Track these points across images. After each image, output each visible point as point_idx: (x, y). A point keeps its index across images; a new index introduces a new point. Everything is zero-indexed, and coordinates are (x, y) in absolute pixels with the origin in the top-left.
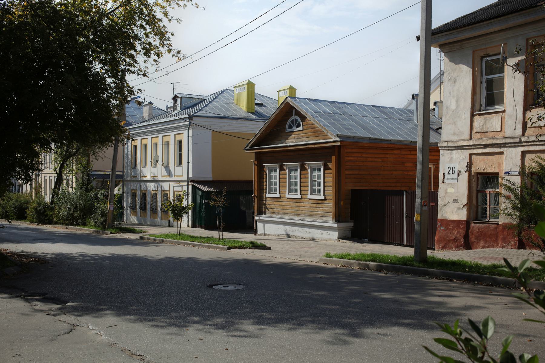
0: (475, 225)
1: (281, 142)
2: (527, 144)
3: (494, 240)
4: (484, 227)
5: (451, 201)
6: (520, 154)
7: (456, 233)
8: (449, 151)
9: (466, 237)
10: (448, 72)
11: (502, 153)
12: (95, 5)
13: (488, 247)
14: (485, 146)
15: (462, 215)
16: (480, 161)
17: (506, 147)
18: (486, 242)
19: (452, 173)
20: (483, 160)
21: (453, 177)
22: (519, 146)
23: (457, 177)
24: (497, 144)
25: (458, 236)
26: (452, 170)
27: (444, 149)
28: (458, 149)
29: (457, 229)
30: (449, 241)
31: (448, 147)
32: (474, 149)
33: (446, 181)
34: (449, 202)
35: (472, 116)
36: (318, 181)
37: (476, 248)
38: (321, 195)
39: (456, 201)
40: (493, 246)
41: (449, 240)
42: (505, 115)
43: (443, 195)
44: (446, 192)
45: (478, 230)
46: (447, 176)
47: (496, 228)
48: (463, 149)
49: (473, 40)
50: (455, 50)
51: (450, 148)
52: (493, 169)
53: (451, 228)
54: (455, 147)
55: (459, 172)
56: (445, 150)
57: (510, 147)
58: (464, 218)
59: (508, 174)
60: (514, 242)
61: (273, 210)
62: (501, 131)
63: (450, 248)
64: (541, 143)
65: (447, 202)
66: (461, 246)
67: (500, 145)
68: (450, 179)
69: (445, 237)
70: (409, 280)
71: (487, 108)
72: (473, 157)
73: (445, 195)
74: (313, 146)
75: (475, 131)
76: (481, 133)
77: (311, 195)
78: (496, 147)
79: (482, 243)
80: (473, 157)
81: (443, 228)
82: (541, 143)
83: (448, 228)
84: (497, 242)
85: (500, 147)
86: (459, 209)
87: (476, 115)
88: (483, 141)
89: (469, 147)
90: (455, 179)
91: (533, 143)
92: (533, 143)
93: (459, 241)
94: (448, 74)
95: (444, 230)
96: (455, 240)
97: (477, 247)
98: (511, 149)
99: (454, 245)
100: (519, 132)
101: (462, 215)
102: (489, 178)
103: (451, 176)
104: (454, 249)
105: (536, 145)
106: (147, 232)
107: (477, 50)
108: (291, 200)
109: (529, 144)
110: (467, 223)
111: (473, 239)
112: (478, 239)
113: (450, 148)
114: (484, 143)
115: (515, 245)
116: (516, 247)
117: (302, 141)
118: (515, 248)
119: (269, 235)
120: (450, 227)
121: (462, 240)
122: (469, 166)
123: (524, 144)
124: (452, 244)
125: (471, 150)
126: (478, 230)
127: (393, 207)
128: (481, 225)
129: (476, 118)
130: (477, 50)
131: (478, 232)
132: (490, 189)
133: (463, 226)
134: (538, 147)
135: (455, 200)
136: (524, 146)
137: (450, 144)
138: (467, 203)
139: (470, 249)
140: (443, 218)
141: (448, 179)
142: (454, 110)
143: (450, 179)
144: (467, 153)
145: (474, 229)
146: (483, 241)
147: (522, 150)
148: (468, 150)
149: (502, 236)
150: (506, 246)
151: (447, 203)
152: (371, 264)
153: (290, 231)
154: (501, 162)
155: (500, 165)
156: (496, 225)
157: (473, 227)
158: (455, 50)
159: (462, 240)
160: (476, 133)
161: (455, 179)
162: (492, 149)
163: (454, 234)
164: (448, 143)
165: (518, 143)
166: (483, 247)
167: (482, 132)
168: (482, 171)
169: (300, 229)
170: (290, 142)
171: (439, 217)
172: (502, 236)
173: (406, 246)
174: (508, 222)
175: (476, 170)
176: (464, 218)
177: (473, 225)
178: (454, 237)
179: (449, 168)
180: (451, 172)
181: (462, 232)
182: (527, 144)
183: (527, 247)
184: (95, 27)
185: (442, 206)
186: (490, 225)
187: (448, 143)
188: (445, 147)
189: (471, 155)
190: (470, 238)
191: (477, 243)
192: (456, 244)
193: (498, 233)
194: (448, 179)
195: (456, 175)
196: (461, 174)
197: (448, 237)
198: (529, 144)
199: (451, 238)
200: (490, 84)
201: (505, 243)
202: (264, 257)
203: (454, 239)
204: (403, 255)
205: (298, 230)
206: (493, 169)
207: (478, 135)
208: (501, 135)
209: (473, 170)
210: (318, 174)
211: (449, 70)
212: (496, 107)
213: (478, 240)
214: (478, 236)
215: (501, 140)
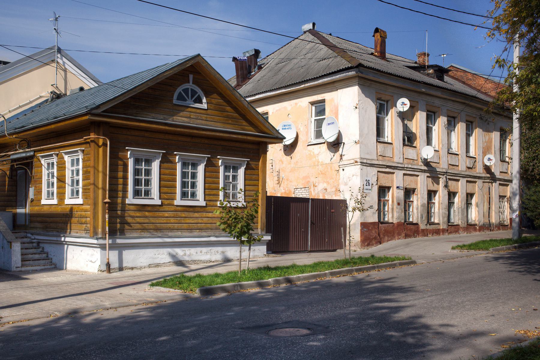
1: (153, 115)
8: (366, 167)
17: (396, 169)
18: (388, 236)
22: (402, 170)
23: (371, 188)
36: (233, 183)
37: (384, 242)
38: (54, 199)
40: (392, 239)
47: (393, 226)
52: (389, 184)
54: (370, 164)
55: (372, 184)
61: (142, 226)
63: (372, 245)
70: (55, 327)
74: (245, 137)
77: (181, 200)
78: (392, 169)
79: (386, 238)
81: (365, 230)
83: (369, 229)
85: (394, 169)
88: (387, 163)
95: (367, 231)
104: (375, 245)
105: (410, 170)
106: (462, 247)
108: (188, 209)
109: (408, 169)
114: (388, 165)
117: (207, 125)
119: (132, 268)
120: (370, 228)
123: (405, 169)
127: (298, 214)
131: (384, 230)
137: (369, 162)
140: (365, 222)
141: (367, 189)
145: (382, 228)
149: (397, 231)
152: (228, 286)
153: (185, 255)
155: (392, 181)
156: (393, 224)
160: (380, 155)
166: (388, 241)
169: (204, 250)
170: (180, 119)
172: (397, 231)
173: (311, 251)
180: (367, 184)
184: (533, 51)
188: (364, 163)
198: (408, 169)
204: (500, 238)
205: (201, 252)
210: (147, 168)
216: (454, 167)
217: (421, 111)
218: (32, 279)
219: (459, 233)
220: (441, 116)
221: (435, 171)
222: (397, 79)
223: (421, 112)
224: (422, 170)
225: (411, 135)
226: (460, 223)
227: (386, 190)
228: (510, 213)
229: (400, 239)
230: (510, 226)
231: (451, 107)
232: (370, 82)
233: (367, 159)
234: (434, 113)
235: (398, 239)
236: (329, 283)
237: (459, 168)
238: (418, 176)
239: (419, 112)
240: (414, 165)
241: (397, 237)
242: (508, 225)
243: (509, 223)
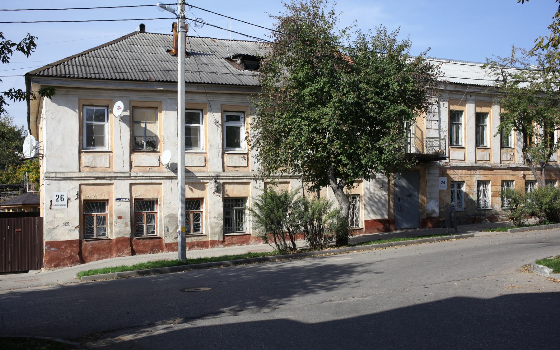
0: (88, 242)
2: (135, 178)
3: (108, 252)
4: (98, 243)
5: (61, 224)
6: (129, 185)
7: (69, 251)
9: (80, 253)
10: (51, 112)
11: (112, 184)
12: (312, 95)
13: (102, 259)
14: (97, 178)
15: (75, 235)
16: (90, 191)
17: (116, 179)
19: (61, 201)
20: (93, 189)
21: (62, 204)
22: (127, 179)
24: (109, 177)
25: (72, 253)
26: (61, 198)
27: (50, 179)
28: (67, 180)
29: (70, 248)
30: (64, 259)
31: (56, 177)
32: (84, 180)
33: (53, 207)
34: (58, 226)
35: (80, 152)
37: (90, 261)
39: (66, 224)
40: (107, 257)
41: (63, 258)
42: (113, 155)
43: (51, 220)
44: (55, 217)
45: (91, 246)
46: (54, 203)
47: (109, 243)
48: (72, 180)
49: (82, 90)
50: (59, 94)
51: (58, 179)
53: (64, 247)
54: (64, 178)
55: (69, 199)
56: (51, 180)
57: (119, 179)
58: (77, 237)
59: (119, 200)
60: (129, 250)
62: (110, 167)
64: (146, 178)
65: (57, 225)
66: (77, 261)
67: (111, 178)
68: (59, 205)
69: (59, 256)
71: (88, 148)
72: (82, 186)
73: (53, 219)
75: (83, 165)
76: (90, 168)
78: (107, 180)
79: (96, 256)
80: (82, 186)
81: (53, 249)
82: (146, 178)
84: (111, 253)
85: (111, 180)
86: (70, 230)
87: (82, 152)
88: (95, 174)
89: (81, 179)
90: (65, 205)
91: (140, 178)
92: (140, 178)
93: (74, 258)
94: (51, 113)
95: (55, 251)
96: (70, 257)
97: (92, 259)
98: (120, 181)
99: (69, 262)
100: (127, 168)
101: (75, 235)
102: (92, 204)
103: (60, 203)
104: (69, 265)
107: (142, 108)
109: (137, 178)
110: (80, 242)
111: (86, 254)
112: (92, 253)
113: (58, 179)
115: (130, 253)
116: (130, 254)
118: (129, 255)
120: (63, 247)
121: (77, 256)
122: (79, 194)
124: (68, 261)
125: (81, 181)
126: (91, 246)
128: (94, 242)
129: (83, 155)
130: (142, 108)
132: (96, 212)
133: (76, 245)
134: (143, 180)
135: (66, 223)
136: (132, 179)
138: (79, 225)
139: (84, 262)
141: (56, 205)
142: (60, 146)
143: (59, 205)
144: (76, 184)
145: (87, 245)
146: (97, 254)
147: (130, 182)
148: (78, 181)
150: (121, 255)
151: (57, 227)
154: (111, 191)
155: (109, 193)
157: (86, 245)
158: (59, 94)
159: (77, 257)
161: (65, 205)
162: (103, 181)
163: (67, 252)
164: (56, 174)
165: (127, 177)
166: (98, 259)
167: (92, 166)
168: (92, 198)
171: (46, 238)
174: (121, 237)
175: (86, 198)
176: (77, 237)
177: (85, 243)
178: (68, 255)
179: (57, 196)
180: (59, 199)
181: (76, 250)
182: (135, 178)
183: (137, 254)
185: (51, 230)
186: (103, 241)
187: (56, 174)
189: (80, 185)
190: (83, 254)
191: (91, 256)
192: (72, 260)
193: (111, 246)
194: (56, 205)
195: (65, 202)
196: (71, 201)
197: (62, 255)
198: (137, 178)
199: (66, 256)
200: (90, 128)
201: (119, 252)
202: (252, 249)
203: (70, 257)
206: (103, 196)
207: (87, 169)
208: (110, 170)
209: (83, 198)
211: (52, 110)
212: (96, 147)
213: (91, 254)
214: (92, 251)
215: (114, 174)
216: (237, 169)
217: (166, 110)
218: (363, 280)
219: (248, 244)
220: (208, 113)
221: (193, 176)
222: (105, 82)
223: (167, 112)
224: (166, 177)
225: (154, 139)
226: (251, 233)
227: (487, 182)
228: (365, 215)
229: (119, 256)
230: (365, 229)
231: (229, 101)
232: (66, 90)
233: (56, 173)
234: (202, 110)
235: (116, 257)
236: (301, 294)
237: (249, 169)
238: (161, 184)
239: (163, 112)
240: (147, 172)
241: (114, 255)
242: (363, 229)
243: (364, 227)
